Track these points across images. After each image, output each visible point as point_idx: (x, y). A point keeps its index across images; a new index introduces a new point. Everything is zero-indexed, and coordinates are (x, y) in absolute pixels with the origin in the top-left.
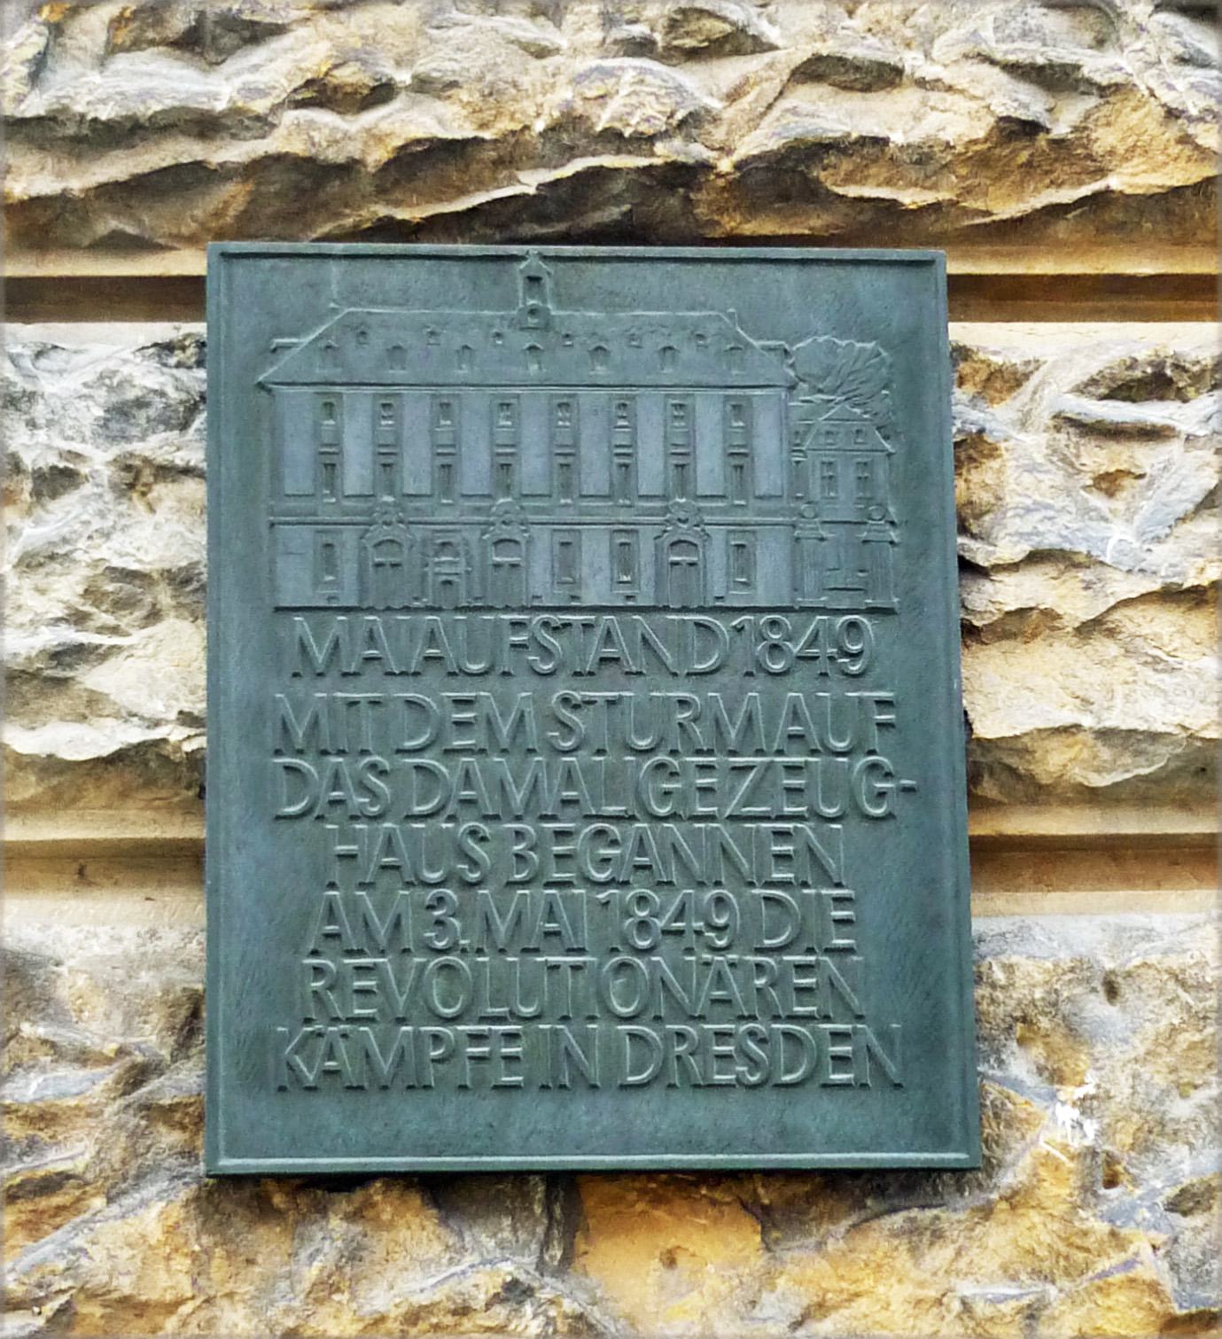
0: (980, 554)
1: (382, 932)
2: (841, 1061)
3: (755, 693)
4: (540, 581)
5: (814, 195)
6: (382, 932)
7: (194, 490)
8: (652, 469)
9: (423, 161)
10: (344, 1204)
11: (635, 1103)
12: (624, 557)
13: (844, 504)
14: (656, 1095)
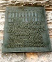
0: (48, 20)
1: (14, 38)
2: (42, 45)
3: (36, 26)
4: (23, 21)
5: (37, 5)
6: (14, 38)
7: (5, 18)
8: (29, 16)
9: (17, 4)
10: (11, 55)
11: (29, 48)
12: (28, 19)
13: (40, 17)
14: (31, 47)
